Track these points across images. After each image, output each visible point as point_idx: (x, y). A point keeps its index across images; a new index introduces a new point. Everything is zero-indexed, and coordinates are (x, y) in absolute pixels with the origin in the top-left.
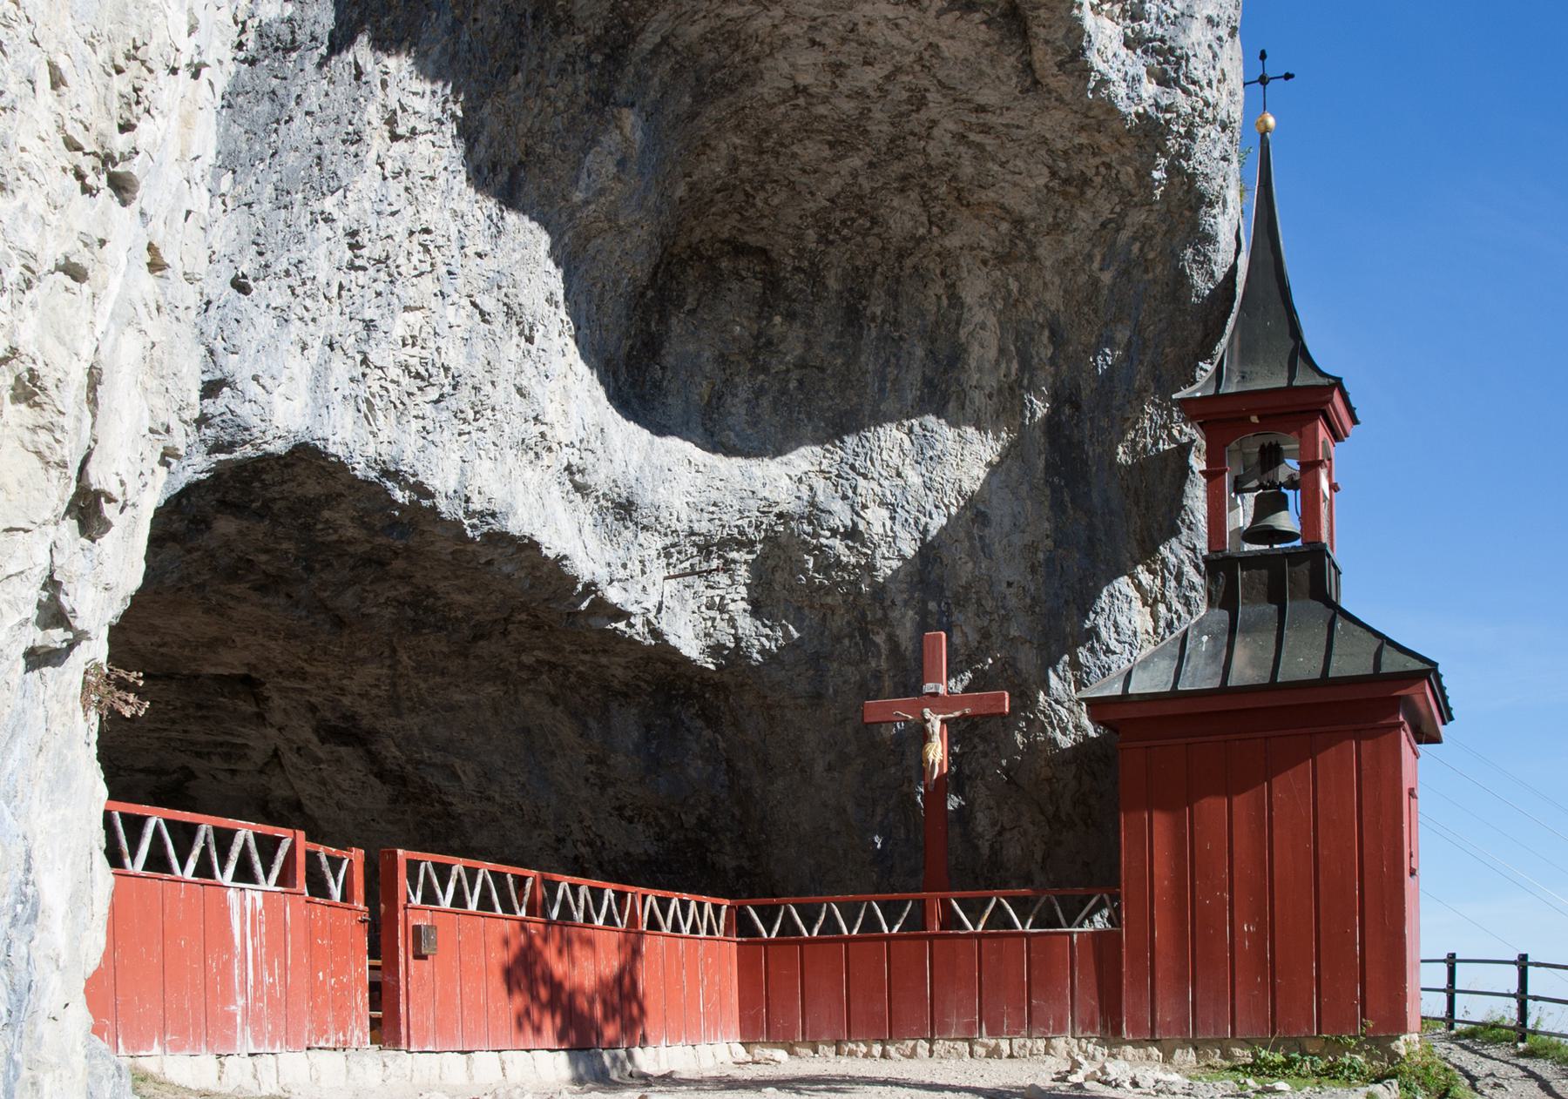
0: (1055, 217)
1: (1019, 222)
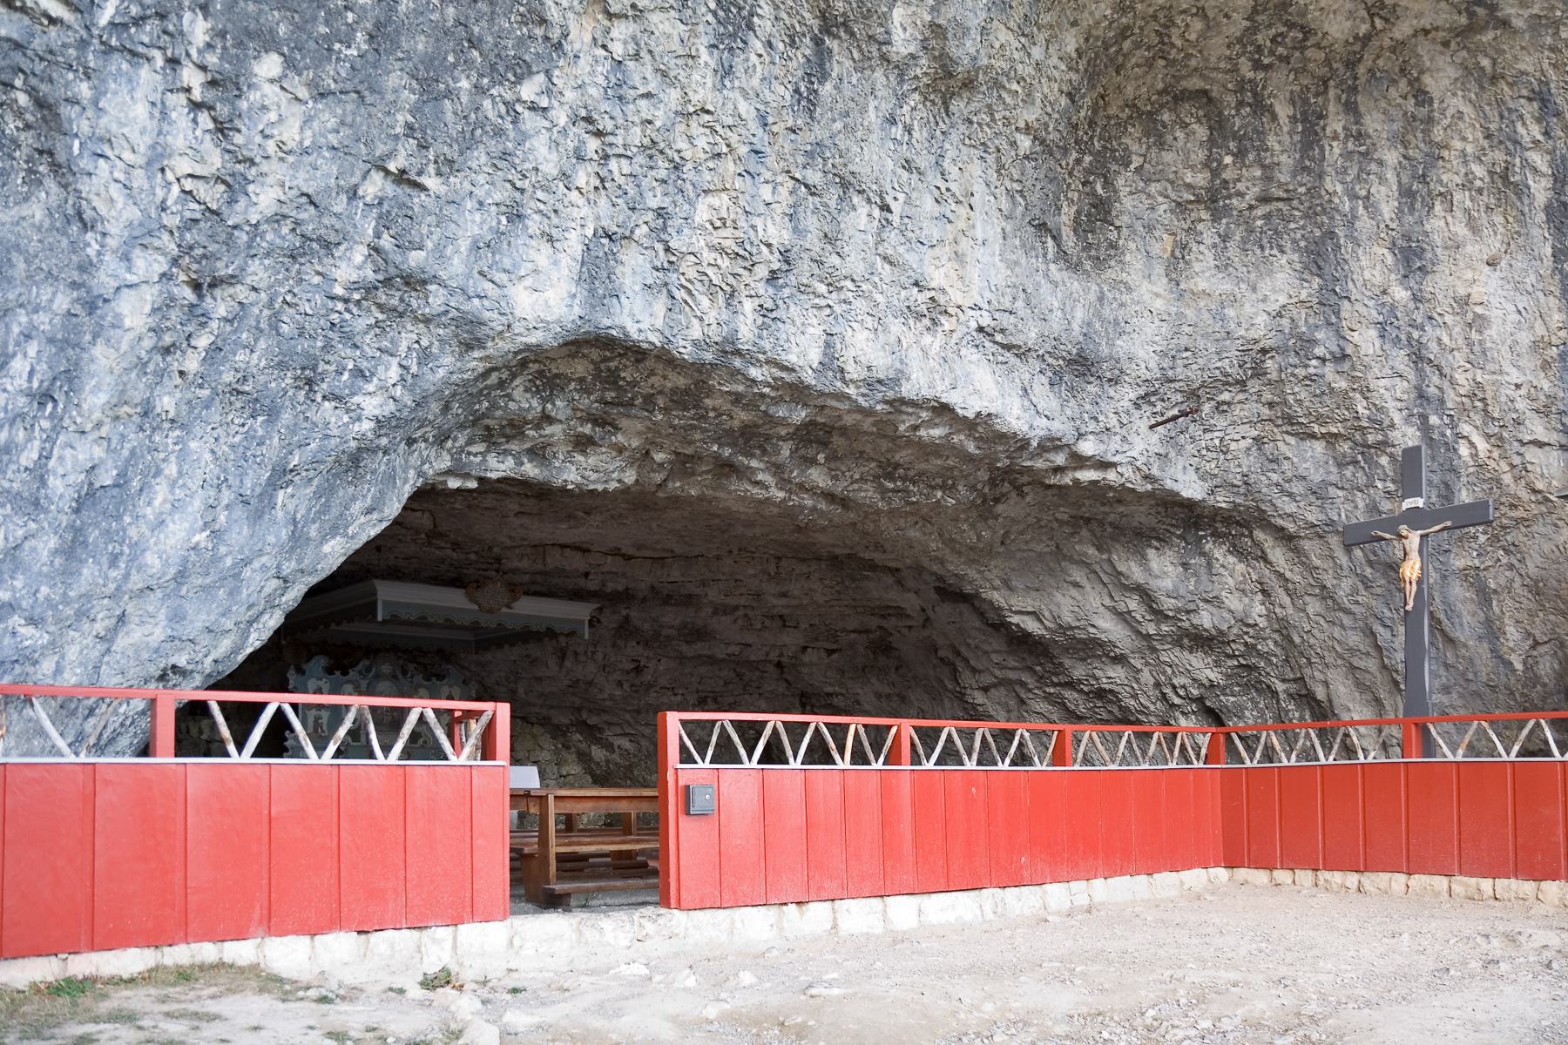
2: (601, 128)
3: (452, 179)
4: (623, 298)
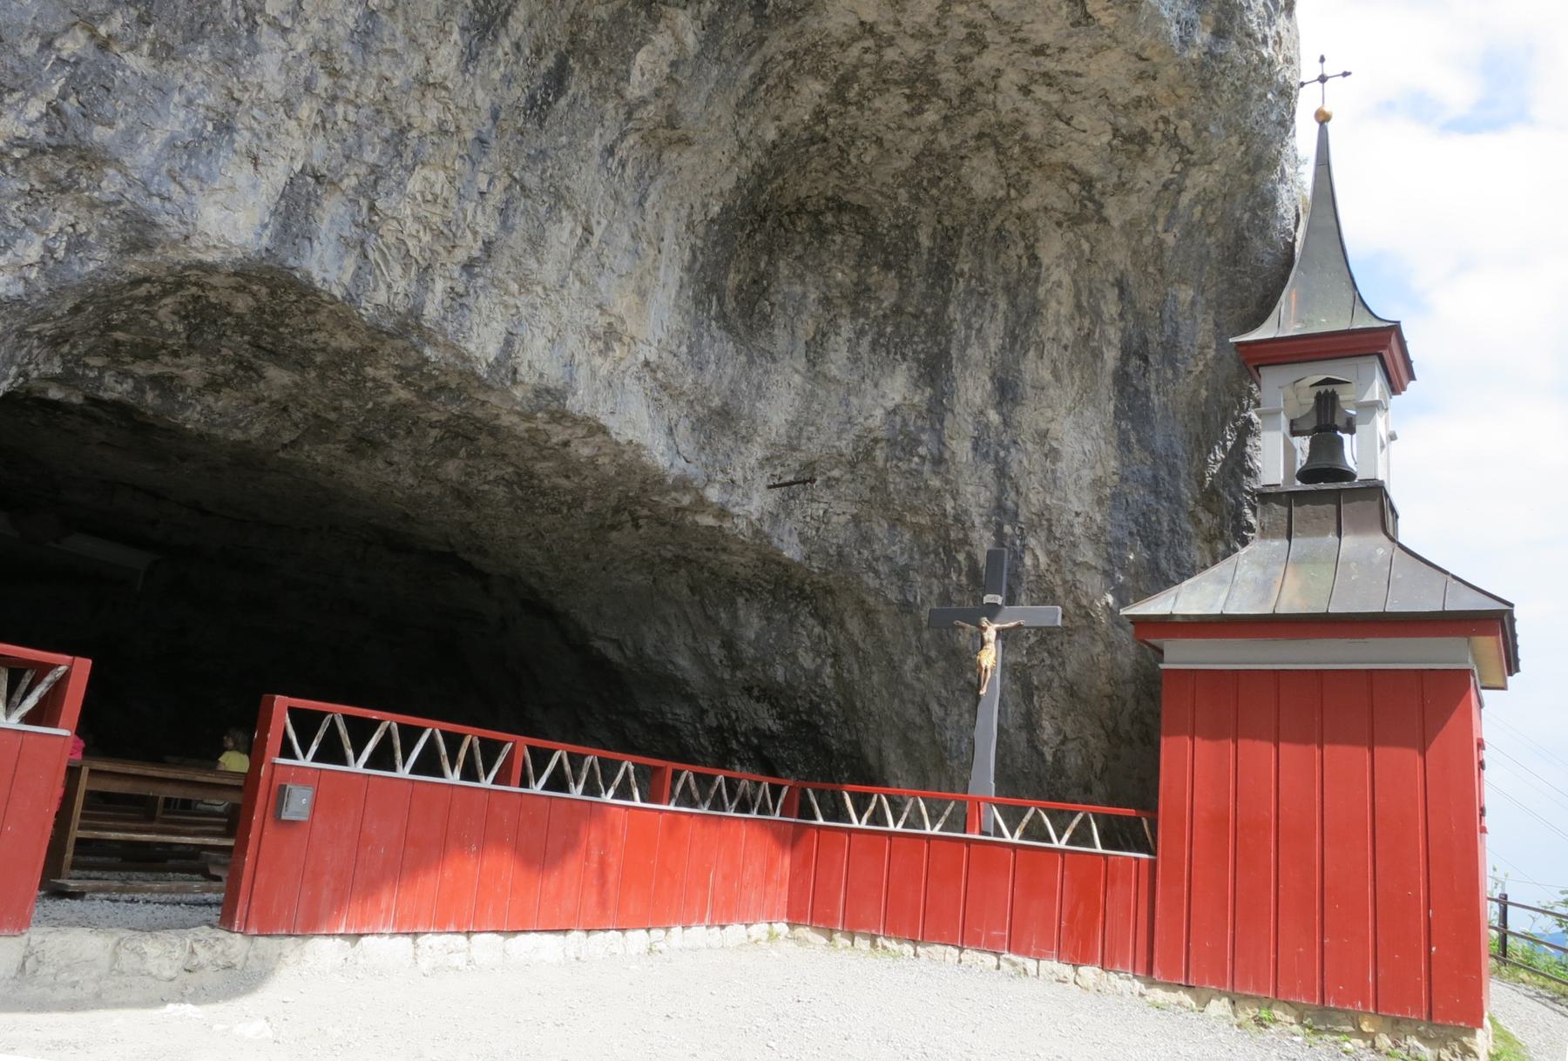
0: (1119, 177)
1: (1087, 183)
2: (338, 67)
3: (165, 65)
4: (315, 243)
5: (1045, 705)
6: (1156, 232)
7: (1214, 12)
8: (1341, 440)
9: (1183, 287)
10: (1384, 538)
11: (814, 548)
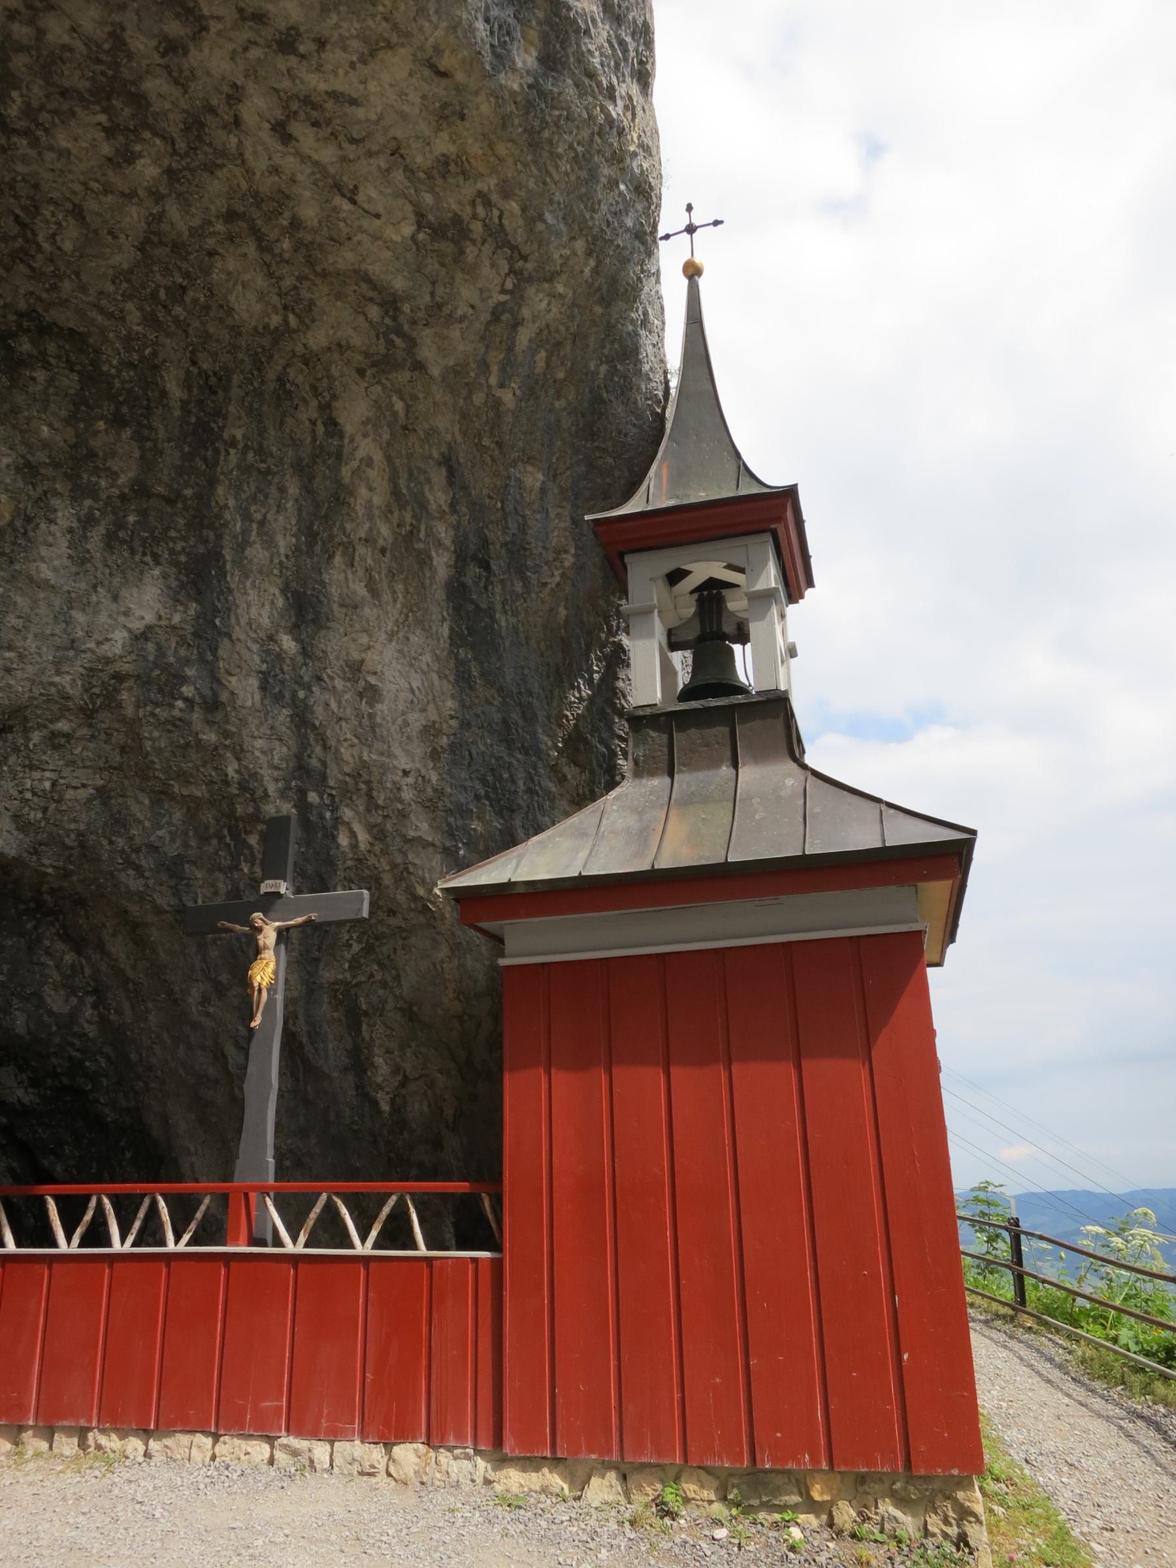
0: (432, 294)
1: (391, 304)
5: (375, 1032)
6: (489, 387)
7: (539, 23)
8: (731, 651)
9: (530, 468)
10: (793, 766)
11: (43, 837)
